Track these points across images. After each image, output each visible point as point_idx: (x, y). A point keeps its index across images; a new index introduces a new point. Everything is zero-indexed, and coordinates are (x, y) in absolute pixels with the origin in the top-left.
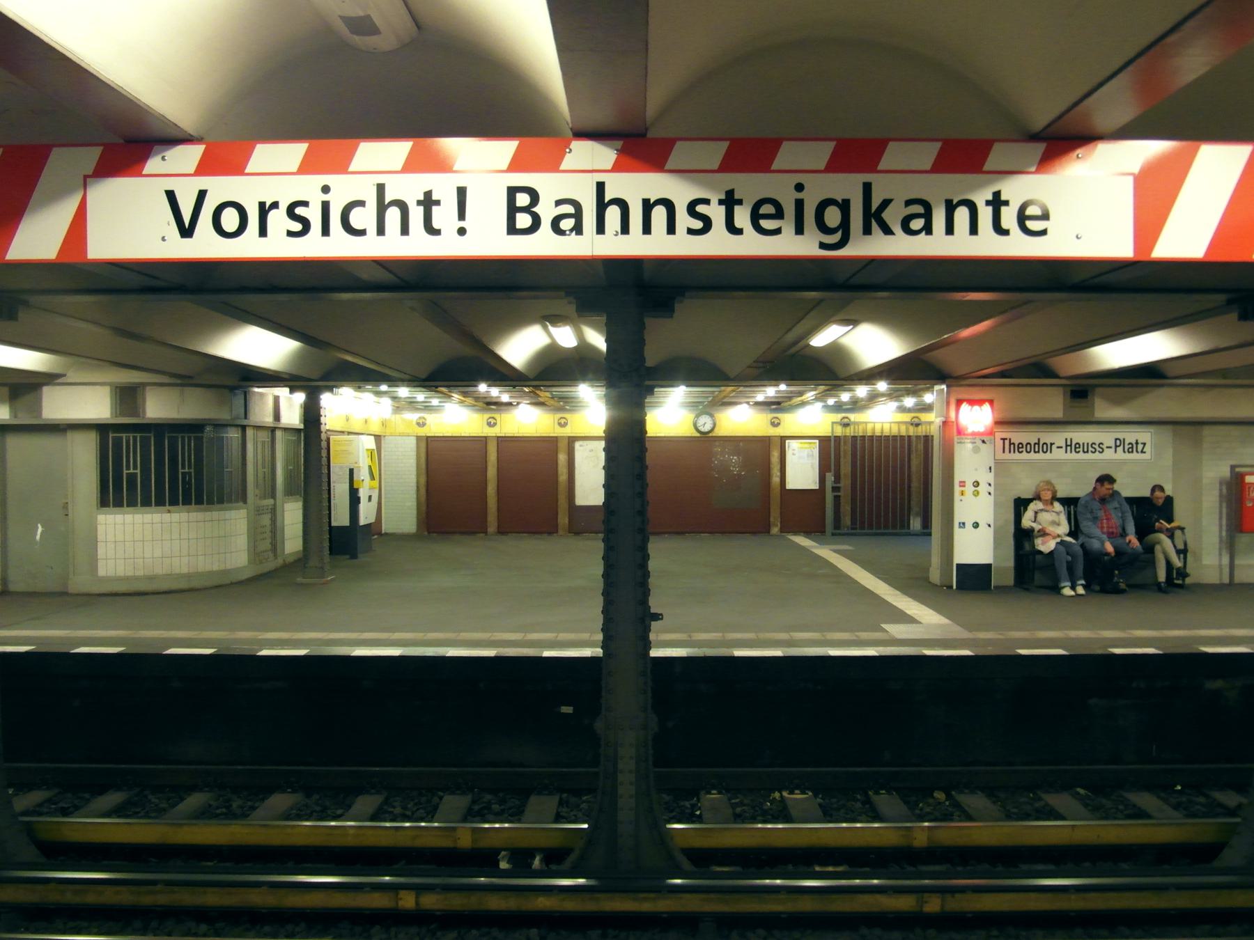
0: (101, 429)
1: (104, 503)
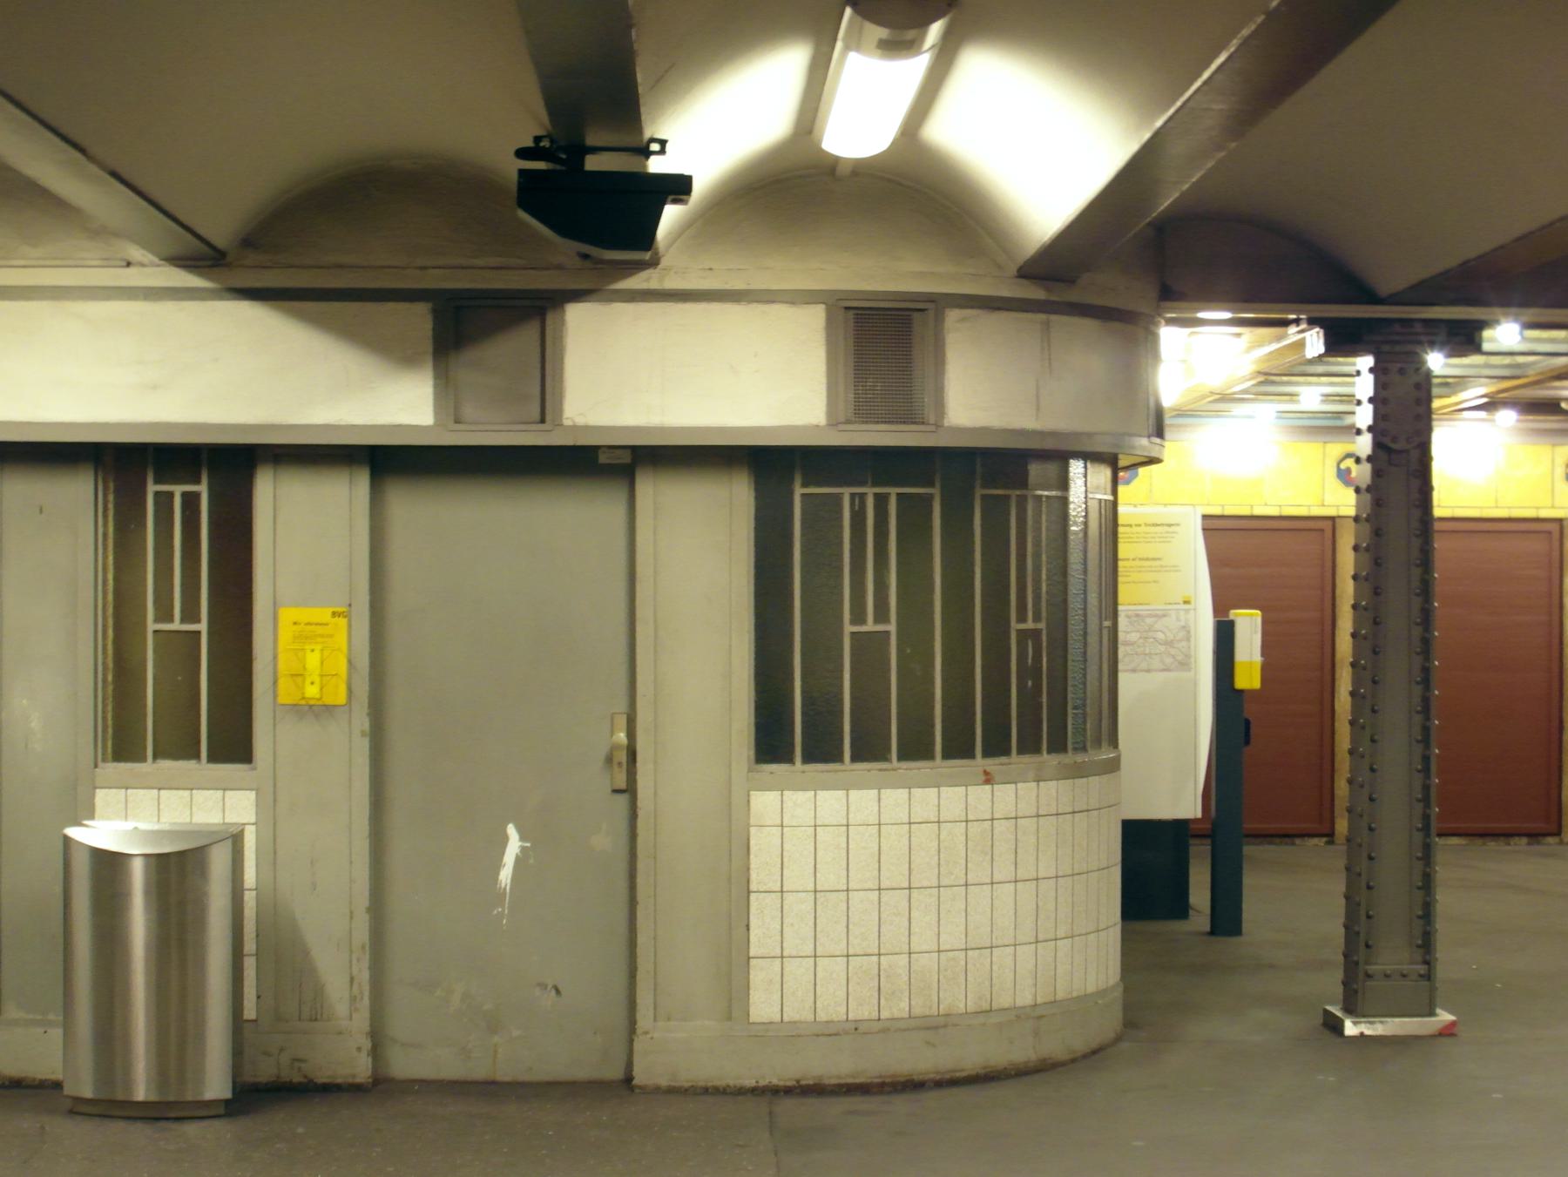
0: (768, 464)
1: (771, 744)
